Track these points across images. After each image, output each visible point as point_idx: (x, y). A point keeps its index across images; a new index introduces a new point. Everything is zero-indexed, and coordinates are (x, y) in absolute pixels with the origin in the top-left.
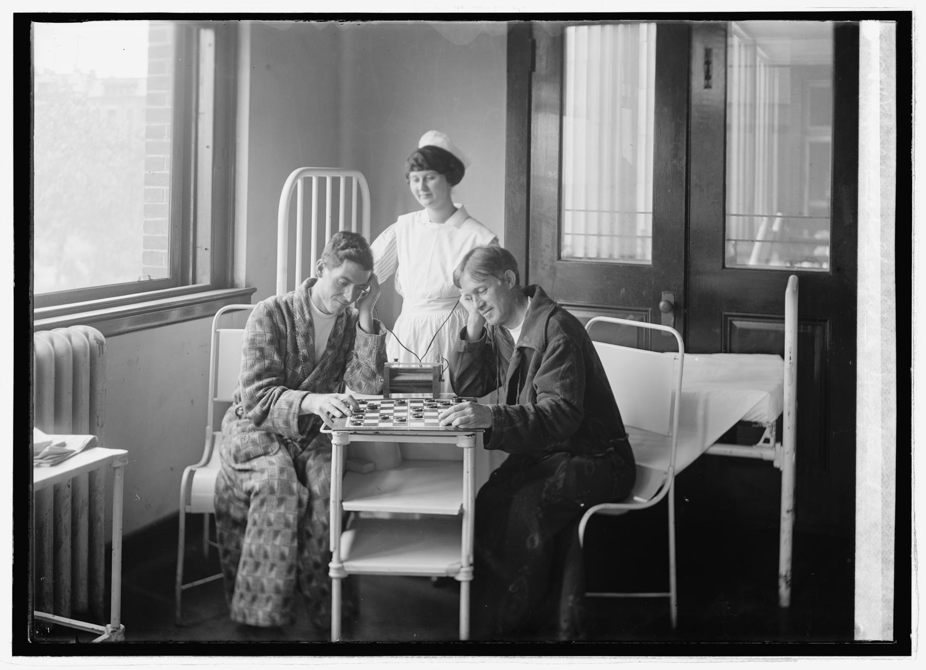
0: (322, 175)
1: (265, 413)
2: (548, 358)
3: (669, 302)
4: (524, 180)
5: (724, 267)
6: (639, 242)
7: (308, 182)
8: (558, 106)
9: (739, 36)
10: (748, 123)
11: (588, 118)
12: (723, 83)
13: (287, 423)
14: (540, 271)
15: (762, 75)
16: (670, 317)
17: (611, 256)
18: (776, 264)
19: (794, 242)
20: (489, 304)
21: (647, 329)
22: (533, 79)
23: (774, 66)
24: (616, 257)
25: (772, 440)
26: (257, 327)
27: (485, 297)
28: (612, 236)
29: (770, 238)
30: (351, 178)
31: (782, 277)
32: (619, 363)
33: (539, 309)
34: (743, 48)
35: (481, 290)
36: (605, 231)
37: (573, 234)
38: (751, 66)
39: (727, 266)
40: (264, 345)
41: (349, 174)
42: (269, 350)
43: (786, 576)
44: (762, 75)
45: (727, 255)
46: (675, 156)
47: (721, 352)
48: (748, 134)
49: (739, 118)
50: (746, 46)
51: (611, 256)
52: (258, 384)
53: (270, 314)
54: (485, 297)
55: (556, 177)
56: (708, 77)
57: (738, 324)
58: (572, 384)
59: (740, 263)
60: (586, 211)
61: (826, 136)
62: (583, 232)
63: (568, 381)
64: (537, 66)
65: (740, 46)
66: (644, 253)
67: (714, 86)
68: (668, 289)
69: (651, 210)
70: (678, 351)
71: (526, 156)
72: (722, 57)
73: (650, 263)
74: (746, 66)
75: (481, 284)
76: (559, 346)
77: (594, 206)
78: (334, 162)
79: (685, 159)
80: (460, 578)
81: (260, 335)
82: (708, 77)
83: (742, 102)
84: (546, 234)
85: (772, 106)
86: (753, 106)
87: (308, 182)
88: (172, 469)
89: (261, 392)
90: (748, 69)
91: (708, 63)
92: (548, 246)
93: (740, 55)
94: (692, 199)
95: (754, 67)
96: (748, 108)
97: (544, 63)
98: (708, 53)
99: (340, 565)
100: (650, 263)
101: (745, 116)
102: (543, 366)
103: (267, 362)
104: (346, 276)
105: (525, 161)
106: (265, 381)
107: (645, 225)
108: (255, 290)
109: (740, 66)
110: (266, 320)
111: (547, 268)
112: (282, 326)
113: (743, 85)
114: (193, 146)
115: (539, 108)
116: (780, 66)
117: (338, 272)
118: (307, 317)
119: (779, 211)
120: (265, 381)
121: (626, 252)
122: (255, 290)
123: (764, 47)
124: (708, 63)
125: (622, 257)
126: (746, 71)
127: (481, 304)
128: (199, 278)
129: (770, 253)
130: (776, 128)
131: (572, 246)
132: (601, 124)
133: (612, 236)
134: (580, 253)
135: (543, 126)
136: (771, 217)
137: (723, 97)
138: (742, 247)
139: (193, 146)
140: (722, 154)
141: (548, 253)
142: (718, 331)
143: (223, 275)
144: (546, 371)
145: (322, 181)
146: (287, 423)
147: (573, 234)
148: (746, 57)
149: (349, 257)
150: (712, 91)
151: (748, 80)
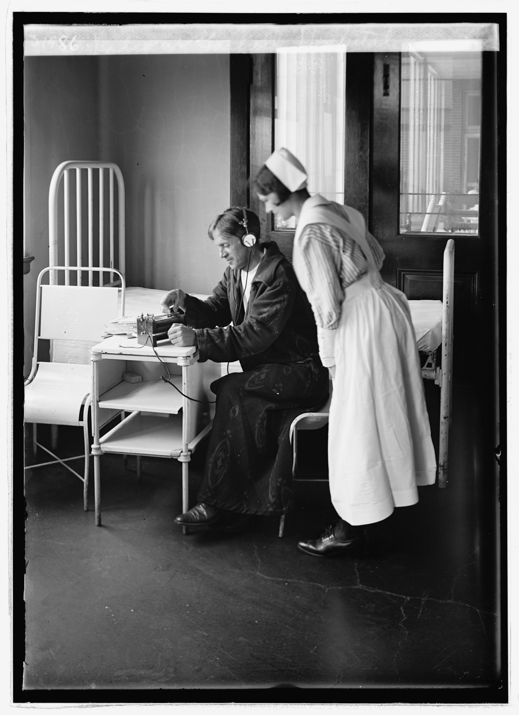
0: (84, 167)
4: (244, 169)
7: (72, 173)
11: (297, 120)
15: (432, 86)
18: (440, 230)
19: (453, 214)
20: (230, 256)
23: (441, 79)
25: (433, 365)
27: (227, 250)
29: (436, 211)
30: (108, 169)
31: (442, 241)
33: (273, 257)
34: (417, 66)
35: (225, 245)
41: (107, 166)
43: (443, 466)
44: (432, 86)
46: (361, 149)
48: (421, 133)
49: (414, 119)
50: (420, 64)
54: (227, 250)
56: (386, 87)
61: (475, 133)
65: (415, 64)
67: (391, 94)
71: (246, 151)
72: (397, 71)
74: (420, 80)
75: (225, 241)
79: (368, 152)
80: (180, 459)
82: (386, 87)
85: (439, 110)
86: (425, 110)
87: (72, 173)
91: (386, 76)
92: (264, 220)
93: (415, 69)
95: (425, 80)
97: (259, 77)
99: (98, 446)
105: (245, 154)
108: (33, 258)
109: (415, 80)
113: (417, 95)
115: (256, 113)
116: (446, 80)
119: (444, 191)
123: (433, 65)
124: (386, 76)
127: (224, 255)
129: (437, 223)
130: (443, 127)
135: (260, 127)
136: (438, 195)
137: (398, 103)
140: (397, 147)
145: (84, 172)
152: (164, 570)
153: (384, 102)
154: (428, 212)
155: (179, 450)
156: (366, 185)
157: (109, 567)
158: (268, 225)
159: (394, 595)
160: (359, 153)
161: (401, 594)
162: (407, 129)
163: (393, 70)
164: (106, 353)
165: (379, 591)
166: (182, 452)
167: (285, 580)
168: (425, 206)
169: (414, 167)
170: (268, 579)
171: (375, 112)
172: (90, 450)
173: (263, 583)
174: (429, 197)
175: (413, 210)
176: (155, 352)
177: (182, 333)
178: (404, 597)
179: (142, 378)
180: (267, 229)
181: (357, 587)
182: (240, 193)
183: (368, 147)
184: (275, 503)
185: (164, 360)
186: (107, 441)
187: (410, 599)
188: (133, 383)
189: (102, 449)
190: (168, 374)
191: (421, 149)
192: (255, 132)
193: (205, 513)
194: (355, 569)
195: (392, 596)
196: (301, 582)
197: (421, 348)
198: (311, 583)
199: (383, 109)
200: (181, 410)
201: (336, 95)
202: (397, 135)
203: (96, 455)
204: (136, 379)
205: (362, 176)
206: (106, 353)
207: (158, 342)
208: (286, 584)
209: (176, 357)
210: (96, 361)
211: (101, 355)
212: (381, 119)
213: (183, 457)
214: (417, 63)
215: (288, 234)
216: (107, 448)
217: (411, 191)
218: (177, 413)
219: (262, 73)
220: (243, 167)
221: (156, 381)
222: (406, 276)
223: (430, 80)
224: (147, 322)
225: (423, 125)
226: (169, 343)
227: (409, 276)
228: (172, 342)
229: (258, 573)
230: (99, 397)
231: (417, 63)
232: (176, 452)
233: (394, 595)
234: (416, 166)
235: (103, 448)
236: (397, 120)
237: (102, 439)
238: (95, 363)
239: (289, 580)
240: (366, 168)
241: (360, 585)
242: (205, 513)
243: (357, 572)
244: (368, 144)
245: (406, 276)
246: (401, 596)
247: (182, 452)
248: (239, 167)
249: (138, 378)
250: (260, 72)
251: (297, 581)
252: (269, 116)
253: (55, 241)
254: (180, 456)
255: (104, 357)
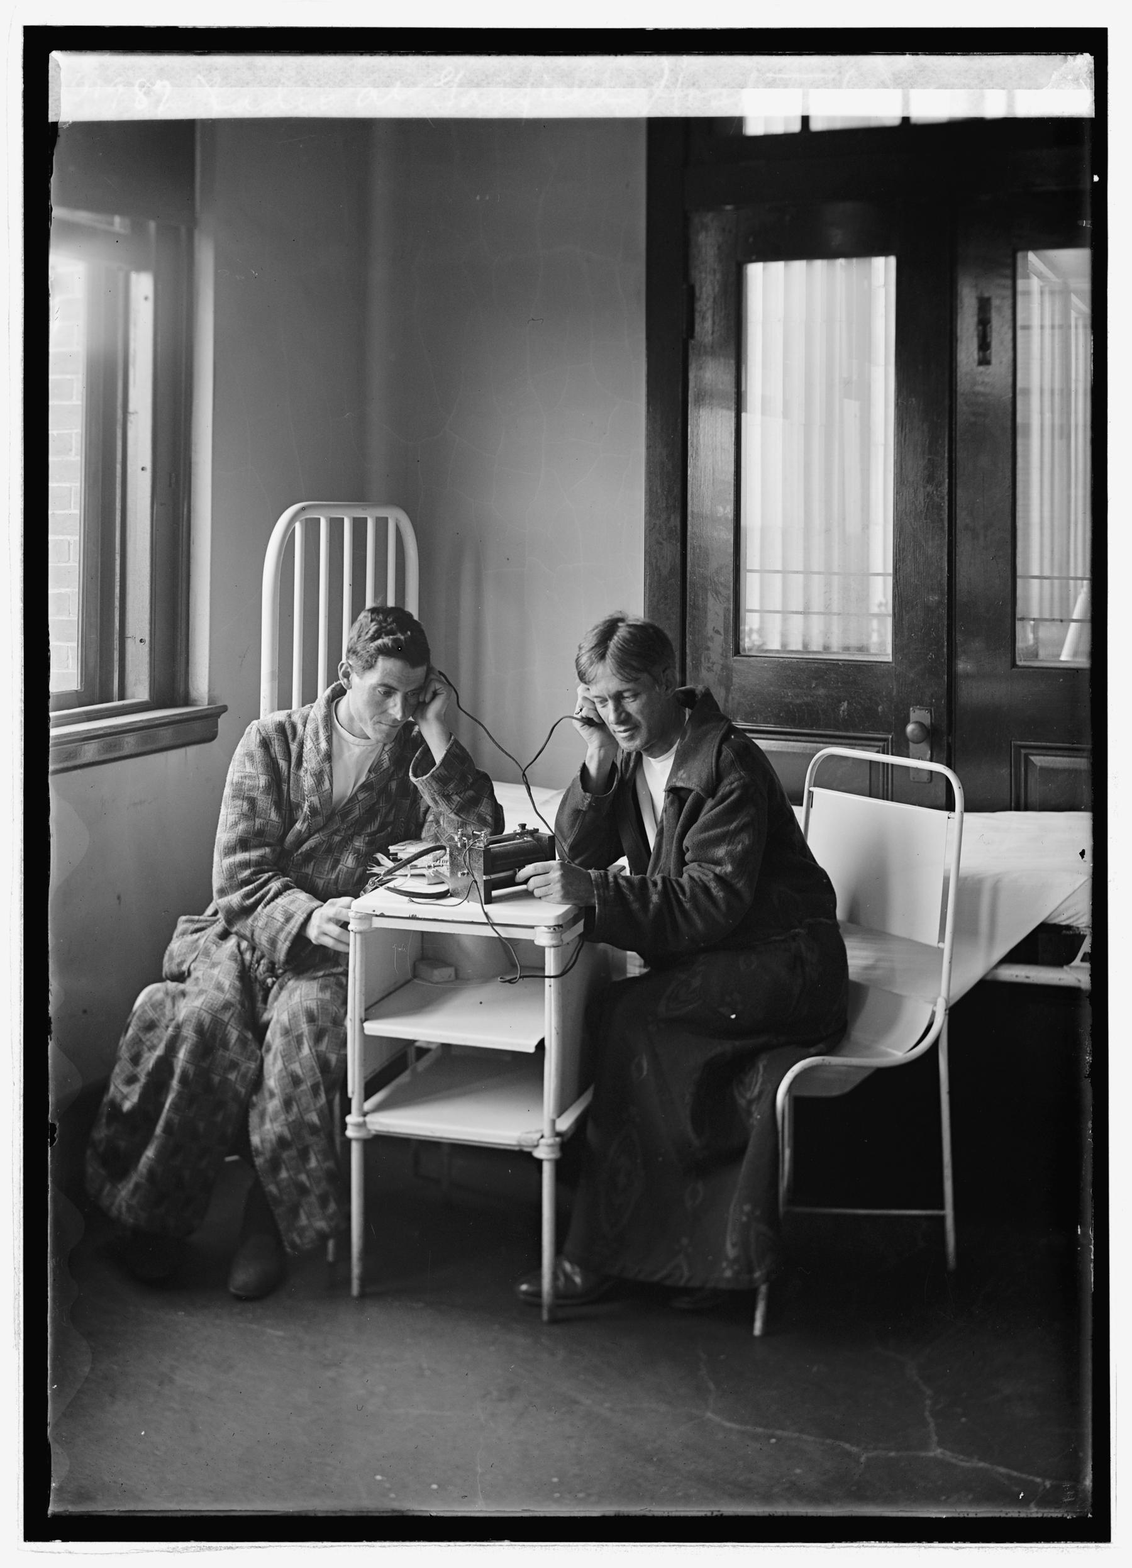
1: (247, 911)
2: (712, 809)
3: (920, 724)
4: (676, 521)
5: (1014, 664)
6: (875, 624)
7: (312, 527)
8: (733, 396)
9: (1040, 276)
10: (1057, 422)
11: (786, 415)
12: (1010, 354)
13: (273, 942)
14: (704, 673)
16: (925, 748)
17: (826, 648)
21: (885, 765)
22: (690, 352)
24: (835, 649)
26: (248, 764)
28: (827, 613)
32: (833, 825)
34: (1047, 297)
36: (817, 605)
37: (762, 611)
38: (1061, 327)
39: (1019, 663)
40: (255, 794)
41: (382, 512)
42: (264, 801)
45: (1019, 645)
46: (930, 479)
47: (1011, 810)
49: (1042, 413)
50: (1052, 293)
51: (826, 648)
52: (241, 856)
53: (265, 744)
55: (731, 516)
56: (984, 345)
57: (1038, 760)
58: (746, 852)
59: (1045, 660)
60: (784, 572)
62: (779, 608)
63: (739, 847)
64: (697, 328)
65: (1042, 293)
66: (879, 642)
67: (994, 361)
68: (920, 703)
69: (890, 570)
70: (954, 810)
72: (1008, 313)
73: (889, 659)
74: (1053, 327)
76: (731, 793)
77: (797, 564)
78: (358, 495)
80: (539, 1154)
81: (250, 777)
82: (984, 345)
83: (1047, 387)
84: (715, 611)
87: (312, 527)
88: (85, 1012)
89: (246, 873)
90: (1057, 331)
91: (984, 323)
92: (717, 632)
94: (959, 550)
96: (1057, 398)
97: (708, 324)
98: (984, 306)
99: (361, 1119)
100: (889, 659)
101: (1052, 412)
102: (702, 819)
103: (258, 821)
104: (386, 682)
105: (677, 490)
106: (254, 855)
107: (881, 593)
108: (224, 709)
109: (1042, 327)
110: (258, 753)
111: (717, 668)
112: (282, 763)
114: (119, 467)
115: (700, 399)
117: (373, 678)
118: (323, 745)
120: (254, 855)
121: (853, 642)
122: (224, 709)
124: (984, 323)
125: (847, 649)
126: (1053, 336)
128: (130, 689)
131: (761, 631)
132: (808, 426)
133: (827, 613)
134: (774, 644)
135: (708, 429)
137: (1010, 379)
138: (1047, 632)
139: (119, 467)
140: (1009, 474)
141: (717, 644)
142: (1005, 772)
143: (171, 684)
144: (706, 828)
145: (336, 526)
146: (273, 942)
147: (762, 611)
148: (1053, 311)
149: (383, 651)
150: (991, 369)
151: (1057, 351)
152: (501, 1400)
153: (979, 379)
154: (1075, 617)
155: (537, 1132)
156: (941, 558)
157: (382, 1388)
158: (726, 643)
159: (1015, 1474)
160: (925, 487)
161: (1030, 1474)
162: (1027, 435)
163: (999, 309)
164: (382, 915)
165: (981, 1464)
166: (542, 1137)
167: (770, 1431)
168: (1068, 606)
169: (1042, 517)
170: (731, 1429)
171: (960, 400)
172: (344, 1126)
173: (720, 1436)
174: (1076, 586)
175: (1041, 612)
176: (486, 914)
177: (562, 875)
178: (1038, 1480)
179: (456, 971)
180: (725, 650)
181: (931, 1454)
182: (665, 572)
183: (946, 476)
184: (736, 1260)
185: (505, 933)
186: (380, 1107)
187: (1052, 1486)
188: (437, 983)
189: (370, 1127)
190: (512, 963)
191: (1057, 478)
192: (698, 441)
193: (578, 1280)
194: (927, 1414)
195: (1009, 1477)
196: (805, 1437)
197: (1069, 918)
198: (828, 1441)
199: (976, 394)
200: (541, 1046)
201: (870, 362)
202: (1010, 450)
203: (357, 1140)
204: (441, 974)
205: (933, 538)
206: (382, 915)
207: (495, 893)
208: (773, 1441)
209: (532, 927)
210: (360, 933)
211: (371, 920)
212: (974, 414)
213: (546, 1149)
214: (1047, 289)
215: (770, 662)
216: (381, 1124)
217: (1035, 571)
218: (532, 1050)
219: (713, 315)
220: (673, 517)
221: (486, 978)
222: (1032, 758)
223: (1076, 327)
224: (470, 849)
225: (1061, 427)
226: (528, 895)
227: (1038, 758)
228: (537, 893)
229: (709, 1415)
230: (366, 1010)
231: (1047, 289)
232: (530, 1136)
233: (1015, 1474)
234: (1047, 514)
235: (373, 1123)
236: (1010, 417)
237: (368, 1105)
238: (358, 936)
239: (779, 1432)
240: (942, 520)
241: (939, 1451)
242: (578, 1280)
243: (930, 1419)
244: (946, 470)
245: (1032, 758)
246: (1031, 1478)
247: (542, 1137)
248: (664, 516)
249: (450, 971)
250: (709, 315)
251: (796, 1435)
252: (729, 408)
253: (273, 673)
254: (537, 1146)
255: (378, 923)
